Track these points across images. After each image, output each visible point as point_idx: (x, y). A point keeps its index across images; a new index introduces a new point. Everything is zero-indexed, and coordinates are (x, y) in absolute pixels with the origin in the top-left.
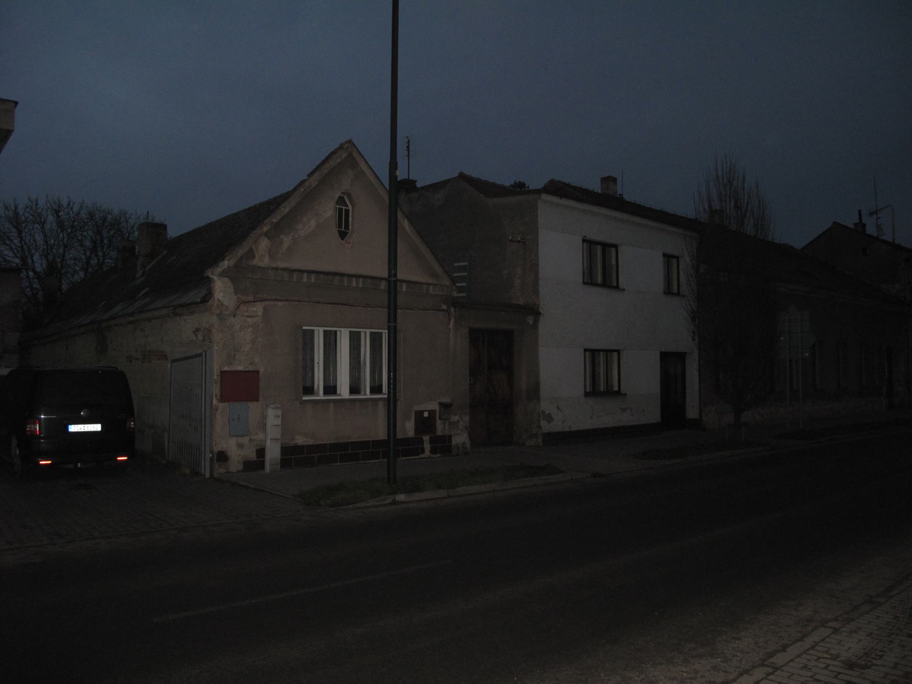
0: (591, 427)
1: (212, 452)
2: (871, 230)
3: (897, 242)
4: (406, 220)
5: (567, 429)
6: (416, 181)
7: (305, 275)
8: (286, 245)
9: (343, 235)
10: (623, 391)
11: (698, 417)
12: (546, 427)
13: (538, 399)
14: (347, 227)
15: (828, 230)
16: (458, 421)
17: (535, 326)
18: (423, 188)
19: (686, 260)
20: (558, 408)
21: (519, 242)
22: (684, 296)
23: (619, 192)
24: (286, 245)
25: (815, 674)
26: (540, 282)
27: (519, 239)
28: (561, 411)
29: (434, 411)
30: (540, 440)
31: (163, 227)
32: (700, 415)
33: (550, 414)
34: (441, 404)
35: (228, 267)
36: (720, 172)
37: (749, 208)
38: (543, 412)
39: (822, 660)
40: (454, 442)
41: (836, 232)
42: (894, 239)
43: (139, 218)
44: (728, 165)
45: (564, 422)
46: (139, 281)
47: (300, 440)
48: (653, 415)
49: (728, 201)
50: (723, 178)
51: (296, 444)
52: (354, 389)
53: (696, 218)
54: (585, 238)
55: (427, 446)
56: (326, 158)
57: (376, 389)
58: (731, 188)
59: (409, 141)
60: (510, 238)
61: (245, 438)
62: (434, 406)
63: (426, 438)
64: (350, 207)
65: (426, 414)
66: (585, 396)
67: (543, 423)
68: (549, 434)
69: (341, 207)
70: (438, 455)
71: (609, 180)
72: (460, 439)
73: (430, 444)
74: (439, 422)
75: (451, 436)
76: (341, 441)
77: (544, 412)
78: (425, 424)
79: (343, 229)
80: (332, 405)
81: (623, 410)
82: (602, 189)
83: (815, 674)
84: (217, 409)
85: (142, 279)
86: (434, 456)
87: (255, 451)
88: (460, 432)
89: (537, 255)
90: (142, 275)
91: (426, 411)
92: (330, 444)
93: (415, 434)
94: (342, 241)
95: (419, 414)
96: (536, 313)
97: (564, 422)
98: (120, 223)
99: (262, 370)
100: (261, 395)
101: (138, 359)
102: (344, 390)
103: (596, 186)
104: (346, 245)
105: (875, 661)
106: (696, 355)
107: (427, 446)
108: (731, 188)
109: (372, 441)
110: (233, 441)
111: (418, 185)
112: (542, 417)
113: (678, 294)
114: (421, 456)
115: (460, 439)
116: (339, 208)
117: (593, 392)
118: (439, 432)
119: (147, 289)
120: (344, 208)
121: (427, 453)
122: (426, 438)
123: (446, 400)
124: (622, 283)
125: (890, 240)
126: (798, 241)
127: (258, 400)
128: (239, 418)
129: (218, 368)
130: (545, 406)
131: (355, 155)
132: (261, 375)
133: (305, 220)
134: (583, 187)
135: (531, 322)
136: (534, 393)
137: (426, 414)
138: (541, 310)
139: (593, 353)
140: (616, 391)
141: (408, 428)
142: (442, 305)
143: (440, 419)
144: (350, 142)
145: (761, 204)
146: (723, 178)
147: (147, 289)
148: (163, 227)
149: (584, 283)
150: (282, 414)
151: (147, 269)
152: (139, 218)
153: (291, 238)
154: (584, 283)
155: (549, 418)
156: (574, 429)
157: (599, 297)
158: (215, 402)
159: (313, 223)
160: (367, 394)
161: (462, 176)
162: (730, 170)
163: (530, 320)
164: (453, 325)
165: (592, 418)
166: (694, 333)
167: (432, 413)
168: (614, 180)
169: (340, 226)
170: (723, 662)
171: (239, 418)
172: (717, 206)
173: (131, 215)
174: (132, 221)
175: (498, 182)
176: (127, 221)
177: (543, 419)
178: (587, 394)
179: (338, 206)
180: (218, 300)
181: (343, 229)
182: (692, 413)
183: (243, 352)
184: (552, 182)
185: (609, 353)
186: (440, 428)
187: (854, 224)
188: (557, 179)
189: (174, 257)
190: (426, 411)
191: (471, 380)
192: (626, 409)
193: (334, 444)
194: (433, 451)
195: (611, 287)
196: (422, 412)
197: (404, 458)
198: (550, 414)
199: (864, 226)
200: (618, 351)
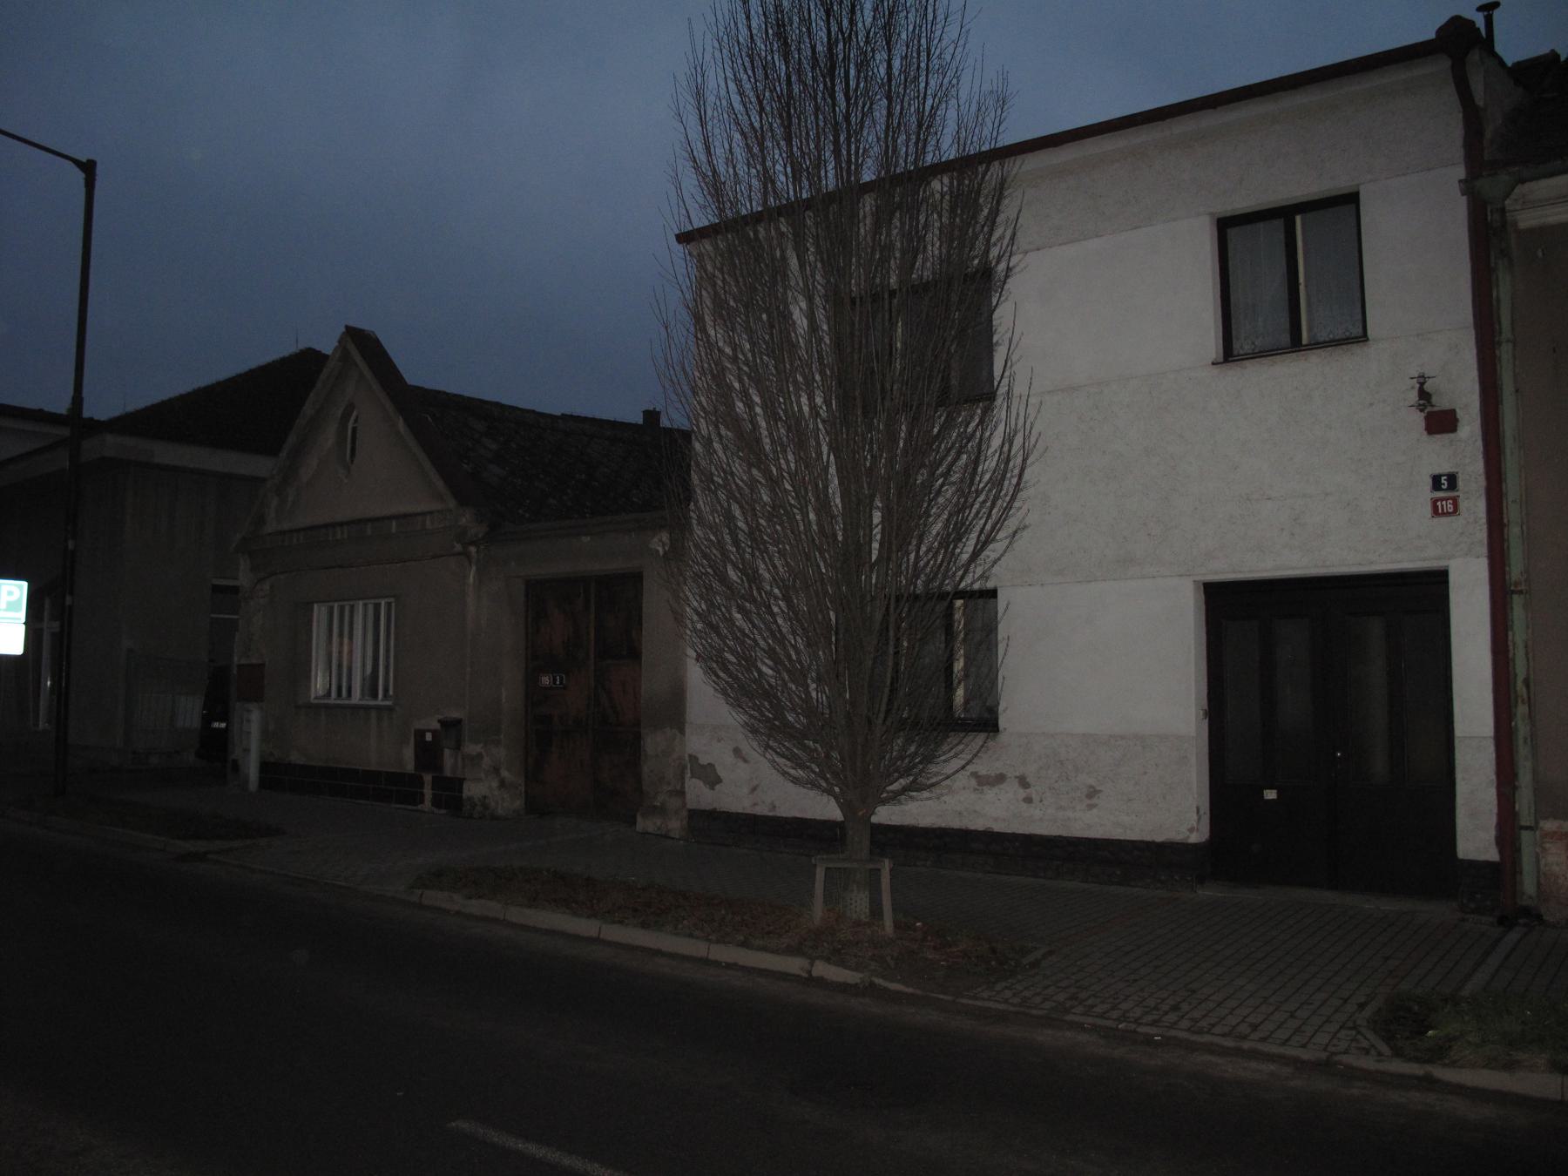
4: (400, 417)
7: (428, 517)
11: (1493, 855)
12: (698, 794)
16: (480, 756)
28: (745, 761)
30: (675, 825)
38: (694, 759)
42: (78, 400)
45: (754, 789)
55: (428, 792)
63: (428, 778)
68: (713, 816)
70: (443, 811)
73: (433, 789)
75: (464, 779)
77: (696, 759)
80: (373, 714)
86: (436, 810)
88: (483, 775)
91: (429, 731)
93: (416, 769)
95: (420, 734)
107: (428, 792)
114: (420, 807)
118: (448, 773)
121: (427, 805)
122: (428, 778)
137: (429, 737)
142: (455, 544)
155: (711, 777)
164: (474, 578)
177: (692, 777)
190: (429, 731)
192: (1000, 778)
193: (393, 773)
194: (437, 802)
197: (398, 806)
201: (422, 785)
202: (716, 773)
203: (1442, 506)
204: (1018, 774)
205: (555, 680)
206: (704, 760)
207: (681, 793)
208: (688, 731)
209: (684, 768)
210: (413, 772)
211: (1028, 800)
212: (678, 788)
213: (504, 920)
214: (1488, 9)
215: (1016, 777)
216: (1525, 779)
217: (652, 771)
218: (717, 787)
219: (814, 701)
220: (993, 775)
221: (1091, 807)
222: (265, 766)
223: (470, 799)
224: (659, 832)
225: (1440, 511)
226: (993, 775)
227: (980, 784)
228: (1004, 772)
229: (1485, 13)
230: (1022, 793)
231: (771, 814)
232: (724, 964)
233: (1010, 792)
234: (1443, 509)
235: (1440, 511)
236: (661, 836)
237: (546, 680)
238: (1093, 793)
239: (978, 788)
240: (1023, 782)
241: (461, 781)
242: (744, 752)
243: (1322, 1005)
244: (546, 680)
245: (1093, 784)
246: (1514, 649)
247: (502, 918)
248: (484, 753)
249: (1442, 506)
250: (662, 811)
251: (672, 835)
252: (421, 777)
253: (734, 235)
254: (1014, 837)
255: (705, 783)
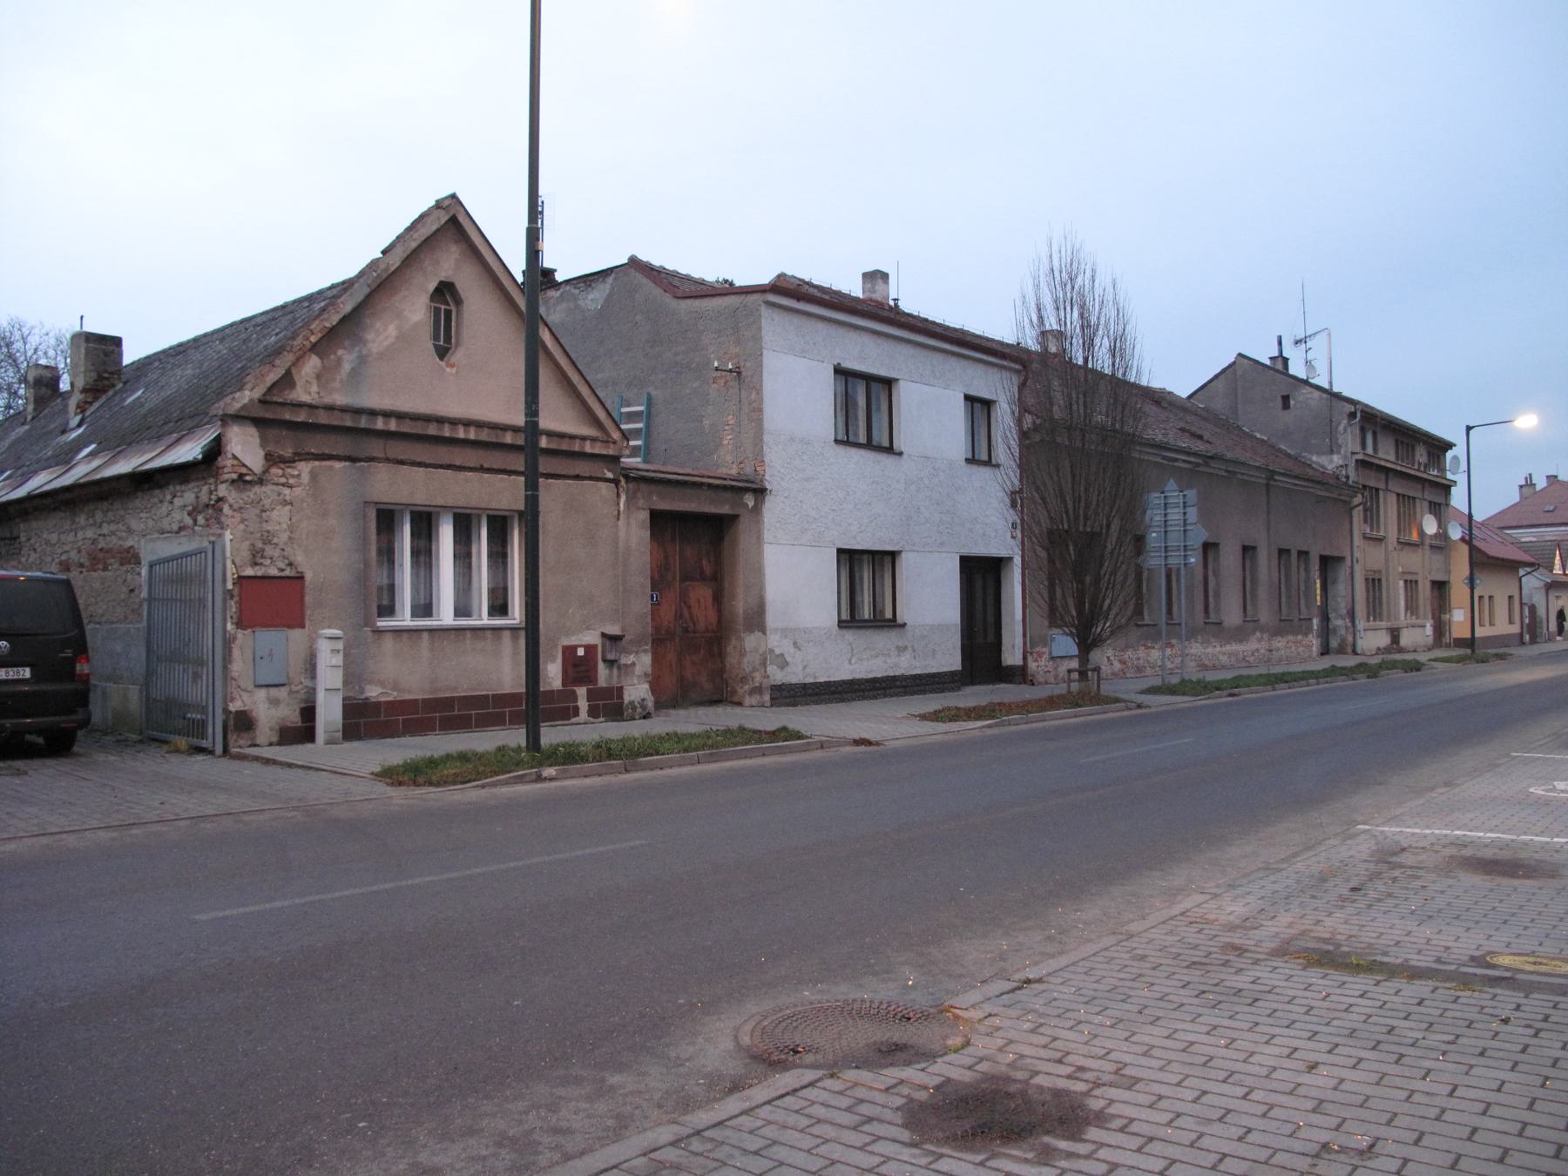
0: (849, 677)
1: (226, 711)
2: (1297, 369)
3: (1336, 389)
5: (810, 680)
6: (555, 270)
8: (347, 367)
9: (442, 353)
10: (900, 620)
13: (762, 628)
14: (448, 338)
15: (1230, 366)
16: (633, 664)
17: (757, 510)
18: (567, 282)
19: (1004, 415)
21: (730, 371)
22: (998, 466)
23: (893, 295)
24: (347, 367)
25: (1184, 938)
26: (766, 438)
27: (730, 367)
29: (594, 647)
30: (767, 698)
31: (117, 342)
32: (1025, 658)
33: (782, 655)
34: (603, 635)
35: (251, 400)
36: (1055, 248)
37: (1102, 322)
38: (772, 651)
39: (1195, 925)
40: (627, 698)
41: (1241, 372)
42: (1331, 383)
43: (47, 334)
44: (1069, 253)
45: (805, 667)
46: (74, 435)
47: (373, 692)
48: (949, 659)
49: (1068, 308)
50: (1061, 272)
51: (367, 699)
52: (462, 610)
53: (1019, 344)
55: (583, 704)
56: (412, 224)
57: (499, 607)
58: (1073, 288)
60: (716, 364)
61: (282, 689)
62: (592, 638)
63: (582, 692)
64: (453, 308)
65: (581, 652)
67: (772, 670)
69: (438, 305)
71: (876, 277)
72: (637, 691)
73: (588, 701)
74: (601, 665)
76: (442, 695)
78: (579, 668)
79: (442, 343)
81: (901, 650)
83: (1184, 938)
84: (235, 638)
85: (81, 430)
87: (298, 711)
88: (635, 681)
89: (759, 392)
90: (79, 425)
92: (423, 700)
94: (441, 363)
95: (569, 651)
96: (760, 492)
97: (805, 667)
98: (12, 343)
99: (309, 576)
100: (307, 617)
101: (82, 565)
102: (446, 615)
103: (853, 287)
104: (448, 370)
105: (1264, 923)
106: (1017, 560)
107: (583, 704)
108: (1073, 288)
109: (493, 695)
110: (262, 694)
111: (559, 277)
113: (988, 463)
114: (574, 720)
115: (637, 691)
116: (435, 308)
117: (851, 621)
119: (93, 446)
120: (443, 307)
123: (614, 630)
125: (1326, 386)
126: (1182, 387)
127: (303, 626)
128: (271, 655)
129: (234, 571)
130: (775, 642)
131: (461, 218)
132: (307, 583)
133: (378, 325)
134: (834, 288)
135: (751, 504)
136: (756, 620)
137: (581, 652)
138: (768, 486)
139: (849, 558)
141: (553, 673)
143: (604, 661)
144: (454, 197)
145: (1121, 315)
146: (1061, 272)
147: (93, 446)
148: (117, 342)
149: (837, 441)
150: (345, 649)
151: (88, 413)
152: (47, 334)
153: (355, 355)
154: (837, 441)
155: (783, 664)
157: (858, 461)
158: (229, 626)
159: (392, 330)
160: (484, 619)
161: (634, 262)
162: (1072, 260)
166: (1014, 526)
167: (590, 649)
168: (884, 276)
169: (436, 337)
170: (1059, 933)
171: (271, 655)
172: (1052, 323)
173: (33, 328)
175: (696, 275)
176: (24, 340)
178: (842, 624)
179: (433, 304)
180: (235, 457)
181: (442, 343)
182: (1012, 655)
183: (276, 544)
184: (782, 276)
186: (603, 675)
187: (1271, 358)
188: (789, 273)
189: (140, 393)
191: (652, 597)
194: (593, 712)
195: (879, 449)
196: (574, 648)
198: (782, 655)
199: (1286, 361)
201: (575, 699)
208: (768, 633)
210: (561, 688)
214: (1565, 1160)
216: (1028, 636)
223: (632, 703)
228: (1202, 542)
233: (907, 656)
241: (620, 690)
243: (785, 1109)
246: (225, 685)
252: (574, 692)
253: (1061, 527)
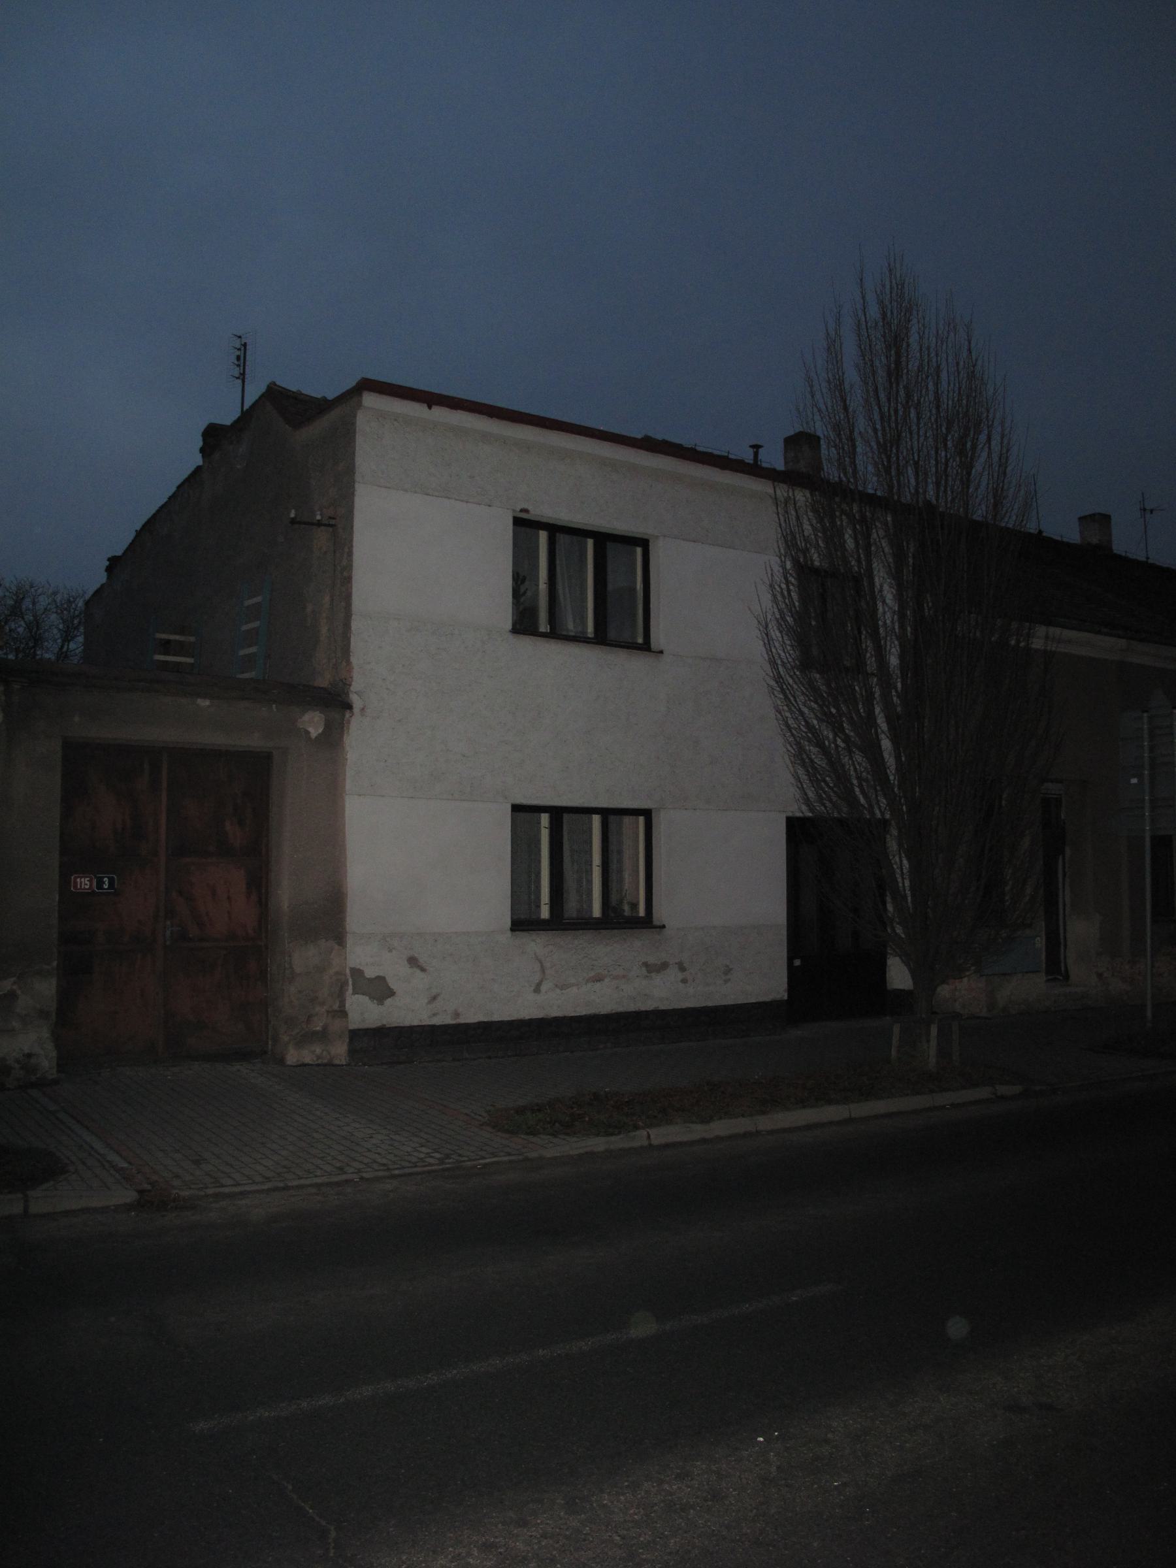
10: (662, 913)
13: (340, 938)
20: (413, 961)
28: (423, 970)
30: (339, 1051)
38: (357, 973)
45: (434, 998)
54: (524, 516)
59: (245, 345)
66: (512, 930)
68: (380, 1033)
81: (652, 969)
82: (786, 463)
112: (350, 983)
124: (659, 637)
140: (544, 921)
155: (381, 990)
156: (471, 1017)
163: (313, 723)
165: (537, 990)
174: (43, 601)
177: (355, 992)
185: (612, 818)
192: (664, 966)
200: (647, 814)
202: (387, 985)
203: (81, 883)
204: (677, 961)
205: (100, 884)
206: (370, 973)
207: (343, 1013)
208: (350, 941)
209: (346, 983)
211: (684, 981)
212: (336, 1007)
213: (757, 1131)
215: (676, 963)
217: (300, 992)
218: (389, 1001)
219: (903, 855)
220: (659, 963)
221: (726, 981)
222: (1153, 838)
224: (320, 1062)
225: (79, 887)
226: (659, 963)
227: (649, 972)
228: (668, 960)
229: (755, 450)
230: (680, 976)
231: (454, 1022)
232: (112, 1208)
233: (673, 974)
234: (81, 886)
235: (79, 887)
236: (325, 1065)
237: (84, 883)
238: (728, 971)
239: (649, 975)
240: (682, 968)
242: (421, 961)
244: (84, 883)
245: (728, 964)
247: (754, 1130)
248: (19, 992)
249: (81, 883)
250: (323, 1036)
251: (337, 1062)
254: (675, 1012)
255: (372, 998)
